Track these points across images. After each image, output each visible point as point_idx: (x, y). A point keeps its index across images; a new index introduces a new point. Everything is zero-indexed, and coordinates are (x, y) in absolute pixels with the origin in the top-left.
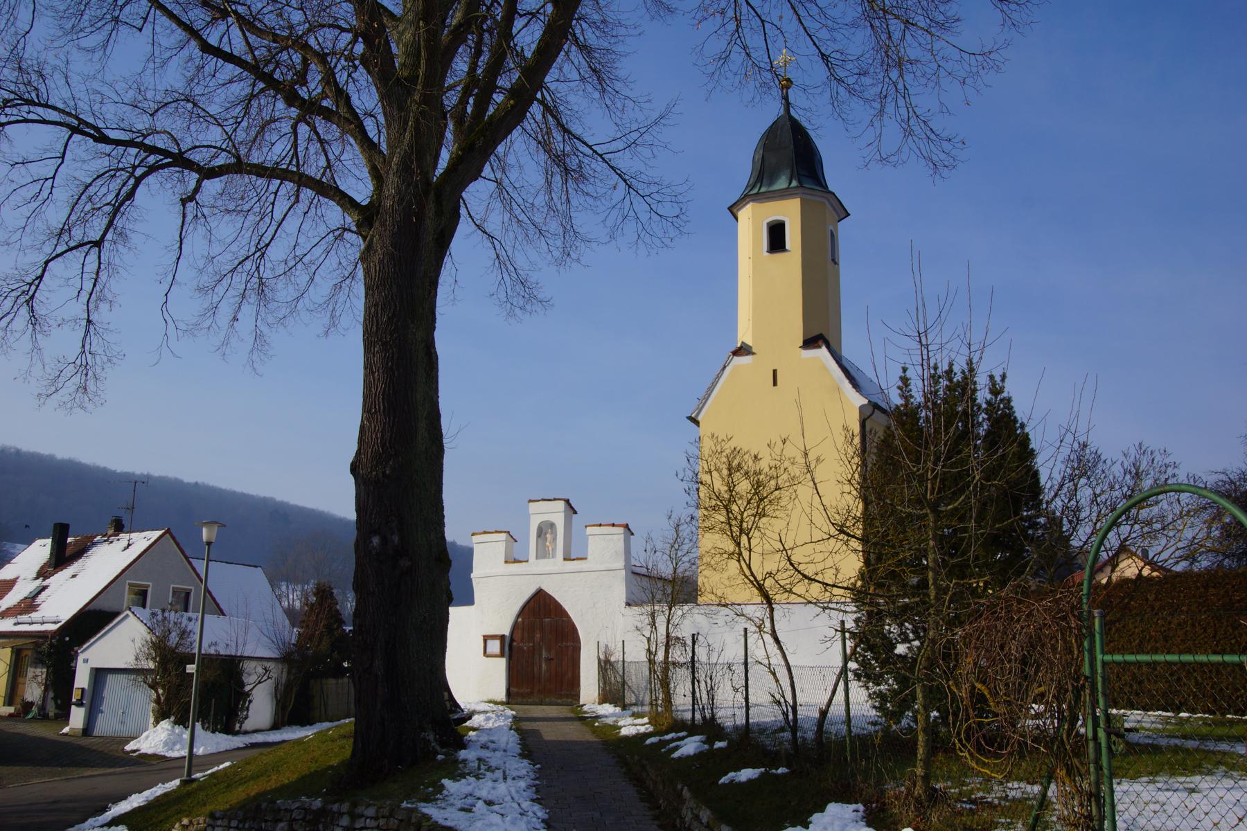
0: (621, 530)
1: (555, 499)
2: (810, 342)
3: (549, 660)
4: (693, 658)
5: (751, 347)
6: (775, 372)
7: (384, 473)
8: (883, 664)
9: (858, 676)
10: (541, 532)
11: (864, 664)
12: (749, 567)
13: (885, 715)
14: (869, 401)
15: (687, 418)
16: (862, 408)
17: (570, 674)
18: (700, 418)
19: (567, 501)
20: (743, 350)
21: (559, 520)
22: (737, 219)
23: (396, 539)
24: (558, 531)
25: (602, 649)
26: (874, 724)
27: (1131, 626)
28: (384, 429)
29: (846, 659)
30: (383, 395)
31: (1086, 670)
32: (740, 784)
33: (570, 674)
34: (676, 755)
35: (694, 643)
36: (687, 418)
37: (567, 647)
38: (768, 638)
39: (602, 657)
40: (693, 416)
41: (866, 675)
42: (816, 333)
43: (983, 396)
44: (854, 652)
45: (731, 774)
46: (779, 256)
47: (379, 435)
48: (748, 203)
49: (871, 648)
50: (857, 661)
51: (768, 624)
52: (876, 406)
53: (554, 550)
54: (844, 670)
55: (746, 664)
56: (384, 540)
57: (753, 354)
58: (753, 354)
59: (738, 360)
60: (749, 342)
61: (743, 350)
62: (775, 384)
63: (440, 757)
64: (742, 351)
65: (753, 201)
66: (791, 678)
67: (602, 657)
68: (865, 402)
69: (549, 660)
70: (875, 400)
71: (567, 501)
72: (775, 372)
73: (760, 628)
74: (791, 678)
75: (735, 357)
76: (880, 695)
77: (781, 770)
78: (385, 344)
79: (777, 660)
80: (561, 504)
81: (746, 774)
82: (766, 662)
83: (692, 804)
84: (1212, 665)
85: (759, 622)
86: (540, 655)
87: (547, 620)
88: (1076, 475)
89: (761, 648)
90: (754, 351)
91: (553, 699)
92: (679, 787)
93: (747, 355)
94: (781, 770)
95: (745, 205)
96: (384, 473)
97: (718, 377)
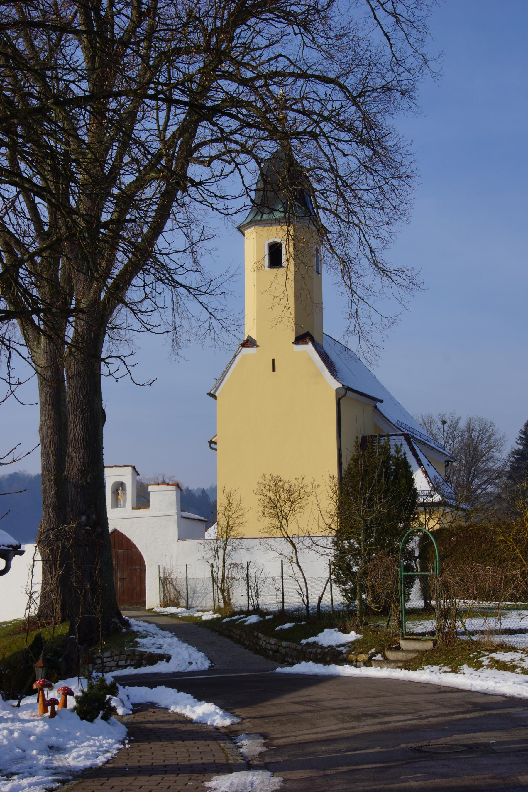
0: (174, 488)
1: (125, 466)
2: (300, 339)
3: (122, 579)
4: (247, 574)
5: (255, 341)
6: (274, 361)
7: (86, 481)
8: (346, 575)
9: (335, 582)
10: (115, 493)
11: (338, 576)
12: (287, 533)
13: (347, 599)
14: (343, 385)
15: (208, 394)
16: (337, 390)
17: (138, 588)
18: (217, 394)
19: (134, 467)
20: (249, 343)
21: (128, 482)
22: (244, 234)
23: (94, 517)
24: (127, 489)
25: (162, 571)
26: (343, 603)
27: (495, 552)
28: (84, 457)
29: (331, 574)
30: (83, 438)
31: (399, 577)
32: (285, 630)
33: (138, 588)
34: (247, 623)
35: (248, 566)
36: (208, 394)
37: (136, 569)
38: (295, 565)
39: (162, 576)
40: (212, 392)
41: (338, 581)
42: (305, 331)
43: (393, 452)
44: (334, 571)
45: (280, 627)
46: (275, 270)
47: (82, 460)
48: (252, 226)
49: (341, 568)
50: (335, 575)
51: (295, 559)
52: (347, 389)
53: (125, 501)
54: (330, 578)
55: (282, 577)
56: (88, 518)
57: (258, 346)
58: (258, 346)
59: (246, 351)
60: (254, 337)
61: (249, 343)
62: (274, 370)
63: (124, 630)
64: (249, 343)
65: (256, 225)
66: (306, 583)
67: (162, 576)
68: (340, 386)
69: (122, 579)
70: (347, 385)
71: (134, 467)
72: (274, 361)
73: (291, 561)
74: (306, 583)
75: (244, 349)
76: (346, 591)
77: (302, 623)
78: (82, 410)
79: (299, 575)
80: (129, 470)
81: (287, 626)
82: (293, 576)
83: (265, 638)
84: (45, 584)
85: (289, 557)
86: (116, 576)
87: (121, 551)
88: (450, 474)
89: (290, 570)
90: (258, 344)
91: (126, 607)
92: (256, 634)
93: (253, 347)
94: (302, 623)
95: (249, 228)
96: (86, 481)
97: (231, 363)
